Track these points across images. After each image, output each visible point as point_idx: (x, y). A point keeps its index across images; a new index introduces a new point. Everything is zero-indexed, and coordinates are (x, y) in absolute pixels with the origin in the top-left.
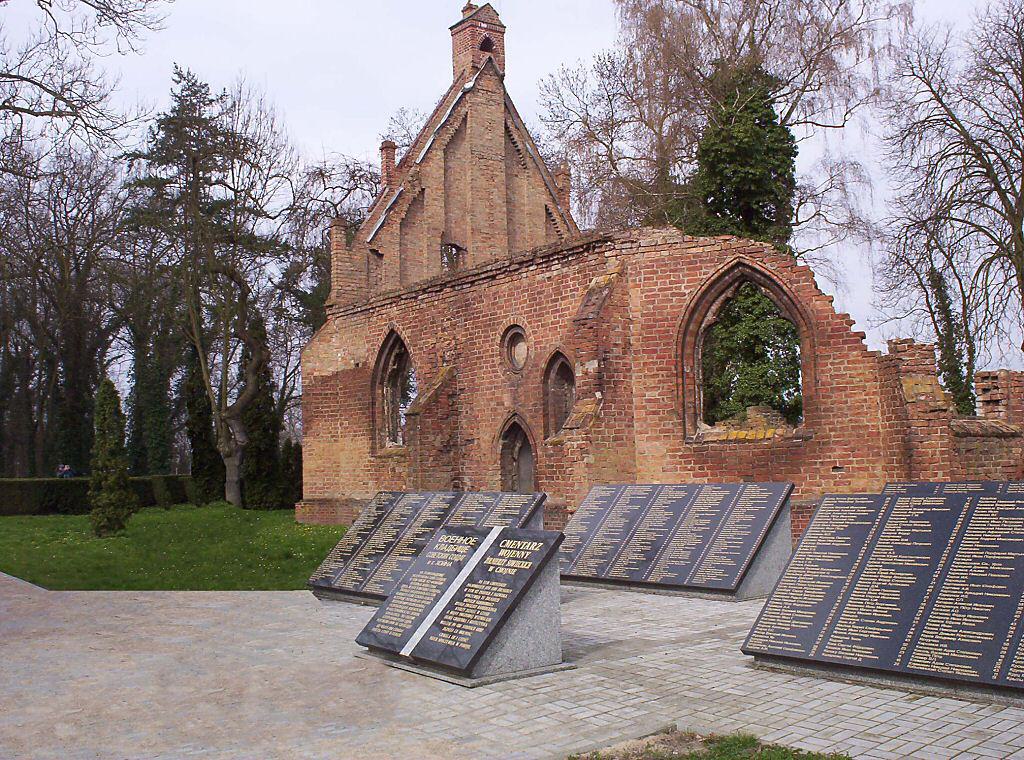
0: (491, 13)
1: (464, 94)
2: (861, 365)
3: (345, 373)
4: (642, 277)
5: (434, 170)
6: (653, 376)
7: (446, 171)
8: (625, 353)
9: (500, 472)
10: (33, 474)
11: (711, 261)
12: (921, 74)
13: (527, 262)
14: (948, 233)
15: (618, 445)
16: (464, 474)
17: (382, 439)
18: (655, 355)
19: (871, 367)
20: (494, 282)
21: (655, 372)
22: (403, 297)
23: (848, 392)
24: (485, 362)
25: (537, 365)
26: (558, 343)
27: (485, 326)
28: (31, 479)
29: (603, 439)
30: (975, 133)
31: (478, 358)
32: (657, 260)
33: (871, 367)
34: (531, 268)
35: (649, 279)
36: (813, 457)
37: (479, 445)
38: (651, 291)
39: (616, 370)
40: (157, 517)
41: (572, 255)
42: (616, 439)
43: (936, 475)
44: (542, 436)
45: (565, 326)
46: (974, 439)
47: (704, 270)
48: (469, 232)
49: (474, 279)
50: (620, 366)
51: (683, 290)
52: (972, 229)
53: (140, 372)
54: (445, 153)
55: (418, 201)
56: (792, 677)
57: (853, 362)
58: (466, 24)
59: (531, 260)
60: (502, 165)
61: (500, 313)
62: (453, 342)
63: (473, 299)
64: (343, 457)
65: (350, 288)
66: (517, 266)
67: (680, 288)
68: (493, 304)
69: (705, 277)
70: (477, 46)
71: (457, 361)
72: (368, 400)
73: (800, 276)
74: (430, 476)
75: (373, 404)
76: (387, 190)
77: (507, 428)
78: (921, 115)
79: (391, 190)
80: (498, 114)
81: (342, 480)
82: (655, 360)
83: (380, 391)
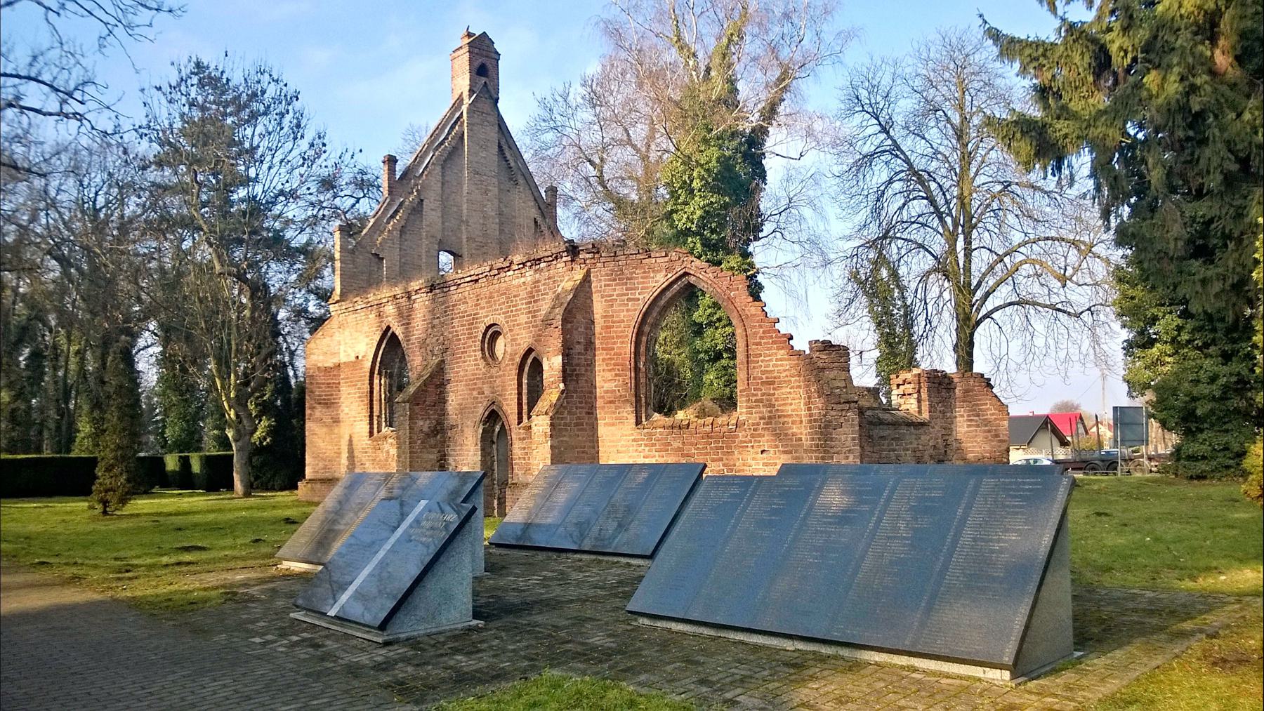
0: (487, 42)
6: (610, 370)
7: (443, 184)
8: (586, 349)
10: (60, 452)
12: (870, 110)
14: (893, 250)
15: (579, 430)
18: (612, 352)
20: (477, 285)
23: (776, 386)
24: (469, 356)
25: (513, 360)
28: (11, 457)
29: (565, 424)
30: (920, 164)
31: (462, 353)
34: (508, 273)
35: (608, 285)
39: (578, 365)
40: (1212, 490)
42: (576, 425)
43: (847, 458)
45: (537, 326)
46: (885, 427)
48: (465, 240)
50: (583, 362)
51: (637, 296)
52: (913, 246)
53: (165, 360)
54: (443, 168)
55: (417, 209)
57: (781, 360)
60: (495, 180)
61: (482, 313)
62: (442, 338)
63: (460, 300)
66: (496, 272)
68: (476, 305)
74: (417, 457)
78: (868, 148)
80: (493, 134)
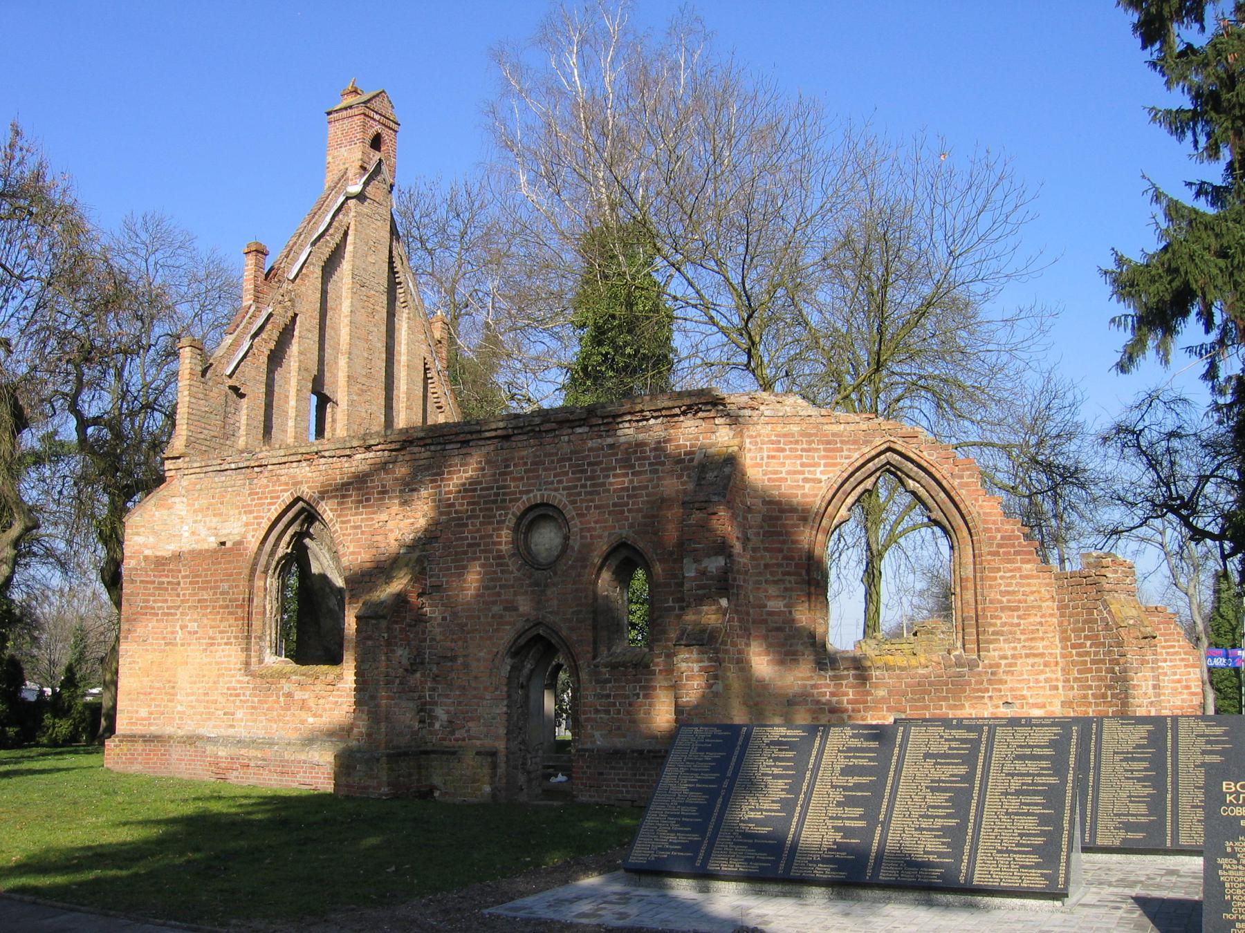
1: (347, 199)
2: (1035, 581)
3: (197, 555)
4: (765, 454)
5: (310, 292)
9: (505, 702)
11: (855, 442)
13: (573, 421)
16: (435, 704)
17: (261, 651)
19: (1047, 585)
20: (506, 445)
21: (780, 577)
22: (327, 454)
26: (624, 533)
27: (485, 502)
32: (785, 435)
33: (1047, 585)
34: (579, 430)
35: (773, 457)
36: (979, 690)
37: (466, 666)
38: (776, 472)
41: (656, 418)
44: (590, 656)
45: (640, 510)
47: (845, 453)
49: (469, 437)
51: (818, 476)
56: (129, 922)
57: (1027, 577)
58: (356, 111)
59: (584, 419)
64: (183, 678)
65: (203, 436)
67: (814, 473)
69: (847, 461)
70: (368, 141)
71: (428, 547)
72: (241, 592)
73: (963, 470)
75: (250, 600)
76: (253, 308)
77: (522, 641)
79: (258, 309)
81: (179, 708)
82: (780, 561)
83: (262, 583)
